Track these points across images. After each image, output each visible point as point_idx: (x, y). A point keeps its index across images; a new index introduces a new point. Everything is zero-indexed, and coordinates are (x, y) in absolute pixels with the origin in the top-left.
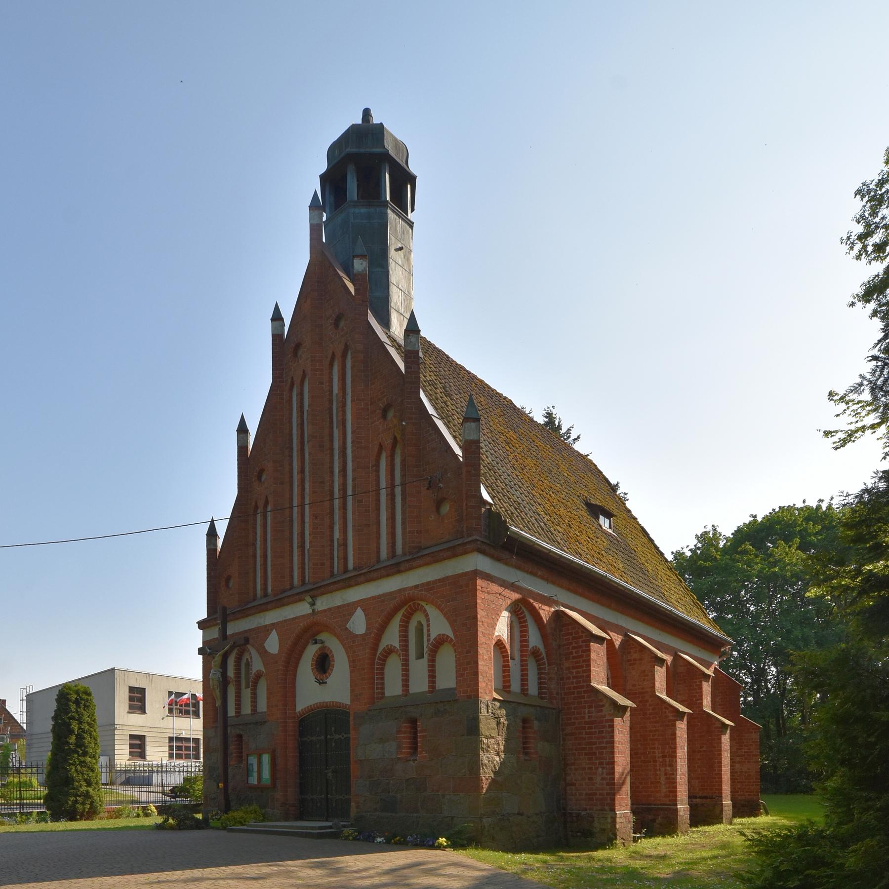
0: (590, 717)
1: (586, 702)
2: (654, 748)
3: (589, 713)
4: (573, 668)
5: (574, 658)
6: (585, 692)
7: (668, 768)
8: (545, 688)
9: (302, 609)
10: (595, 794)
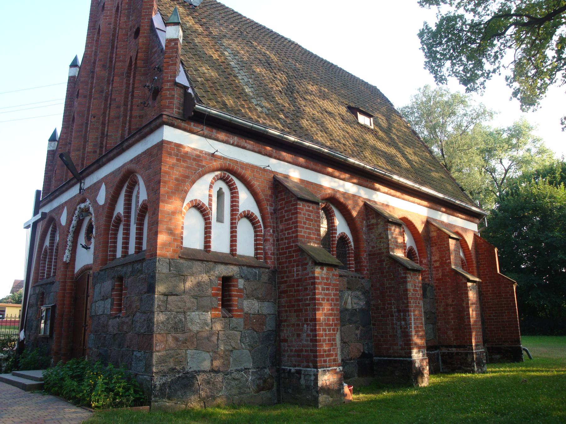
0: (298, 275)
1: (295, 261)
2: (391, 304)
3: (297, 271)
4: (286, 230)
5: (286, 220)
6: (294, 251)
7: (403, 323)
8: (261, 249)
9: (74, 191)
10: (302, 351)
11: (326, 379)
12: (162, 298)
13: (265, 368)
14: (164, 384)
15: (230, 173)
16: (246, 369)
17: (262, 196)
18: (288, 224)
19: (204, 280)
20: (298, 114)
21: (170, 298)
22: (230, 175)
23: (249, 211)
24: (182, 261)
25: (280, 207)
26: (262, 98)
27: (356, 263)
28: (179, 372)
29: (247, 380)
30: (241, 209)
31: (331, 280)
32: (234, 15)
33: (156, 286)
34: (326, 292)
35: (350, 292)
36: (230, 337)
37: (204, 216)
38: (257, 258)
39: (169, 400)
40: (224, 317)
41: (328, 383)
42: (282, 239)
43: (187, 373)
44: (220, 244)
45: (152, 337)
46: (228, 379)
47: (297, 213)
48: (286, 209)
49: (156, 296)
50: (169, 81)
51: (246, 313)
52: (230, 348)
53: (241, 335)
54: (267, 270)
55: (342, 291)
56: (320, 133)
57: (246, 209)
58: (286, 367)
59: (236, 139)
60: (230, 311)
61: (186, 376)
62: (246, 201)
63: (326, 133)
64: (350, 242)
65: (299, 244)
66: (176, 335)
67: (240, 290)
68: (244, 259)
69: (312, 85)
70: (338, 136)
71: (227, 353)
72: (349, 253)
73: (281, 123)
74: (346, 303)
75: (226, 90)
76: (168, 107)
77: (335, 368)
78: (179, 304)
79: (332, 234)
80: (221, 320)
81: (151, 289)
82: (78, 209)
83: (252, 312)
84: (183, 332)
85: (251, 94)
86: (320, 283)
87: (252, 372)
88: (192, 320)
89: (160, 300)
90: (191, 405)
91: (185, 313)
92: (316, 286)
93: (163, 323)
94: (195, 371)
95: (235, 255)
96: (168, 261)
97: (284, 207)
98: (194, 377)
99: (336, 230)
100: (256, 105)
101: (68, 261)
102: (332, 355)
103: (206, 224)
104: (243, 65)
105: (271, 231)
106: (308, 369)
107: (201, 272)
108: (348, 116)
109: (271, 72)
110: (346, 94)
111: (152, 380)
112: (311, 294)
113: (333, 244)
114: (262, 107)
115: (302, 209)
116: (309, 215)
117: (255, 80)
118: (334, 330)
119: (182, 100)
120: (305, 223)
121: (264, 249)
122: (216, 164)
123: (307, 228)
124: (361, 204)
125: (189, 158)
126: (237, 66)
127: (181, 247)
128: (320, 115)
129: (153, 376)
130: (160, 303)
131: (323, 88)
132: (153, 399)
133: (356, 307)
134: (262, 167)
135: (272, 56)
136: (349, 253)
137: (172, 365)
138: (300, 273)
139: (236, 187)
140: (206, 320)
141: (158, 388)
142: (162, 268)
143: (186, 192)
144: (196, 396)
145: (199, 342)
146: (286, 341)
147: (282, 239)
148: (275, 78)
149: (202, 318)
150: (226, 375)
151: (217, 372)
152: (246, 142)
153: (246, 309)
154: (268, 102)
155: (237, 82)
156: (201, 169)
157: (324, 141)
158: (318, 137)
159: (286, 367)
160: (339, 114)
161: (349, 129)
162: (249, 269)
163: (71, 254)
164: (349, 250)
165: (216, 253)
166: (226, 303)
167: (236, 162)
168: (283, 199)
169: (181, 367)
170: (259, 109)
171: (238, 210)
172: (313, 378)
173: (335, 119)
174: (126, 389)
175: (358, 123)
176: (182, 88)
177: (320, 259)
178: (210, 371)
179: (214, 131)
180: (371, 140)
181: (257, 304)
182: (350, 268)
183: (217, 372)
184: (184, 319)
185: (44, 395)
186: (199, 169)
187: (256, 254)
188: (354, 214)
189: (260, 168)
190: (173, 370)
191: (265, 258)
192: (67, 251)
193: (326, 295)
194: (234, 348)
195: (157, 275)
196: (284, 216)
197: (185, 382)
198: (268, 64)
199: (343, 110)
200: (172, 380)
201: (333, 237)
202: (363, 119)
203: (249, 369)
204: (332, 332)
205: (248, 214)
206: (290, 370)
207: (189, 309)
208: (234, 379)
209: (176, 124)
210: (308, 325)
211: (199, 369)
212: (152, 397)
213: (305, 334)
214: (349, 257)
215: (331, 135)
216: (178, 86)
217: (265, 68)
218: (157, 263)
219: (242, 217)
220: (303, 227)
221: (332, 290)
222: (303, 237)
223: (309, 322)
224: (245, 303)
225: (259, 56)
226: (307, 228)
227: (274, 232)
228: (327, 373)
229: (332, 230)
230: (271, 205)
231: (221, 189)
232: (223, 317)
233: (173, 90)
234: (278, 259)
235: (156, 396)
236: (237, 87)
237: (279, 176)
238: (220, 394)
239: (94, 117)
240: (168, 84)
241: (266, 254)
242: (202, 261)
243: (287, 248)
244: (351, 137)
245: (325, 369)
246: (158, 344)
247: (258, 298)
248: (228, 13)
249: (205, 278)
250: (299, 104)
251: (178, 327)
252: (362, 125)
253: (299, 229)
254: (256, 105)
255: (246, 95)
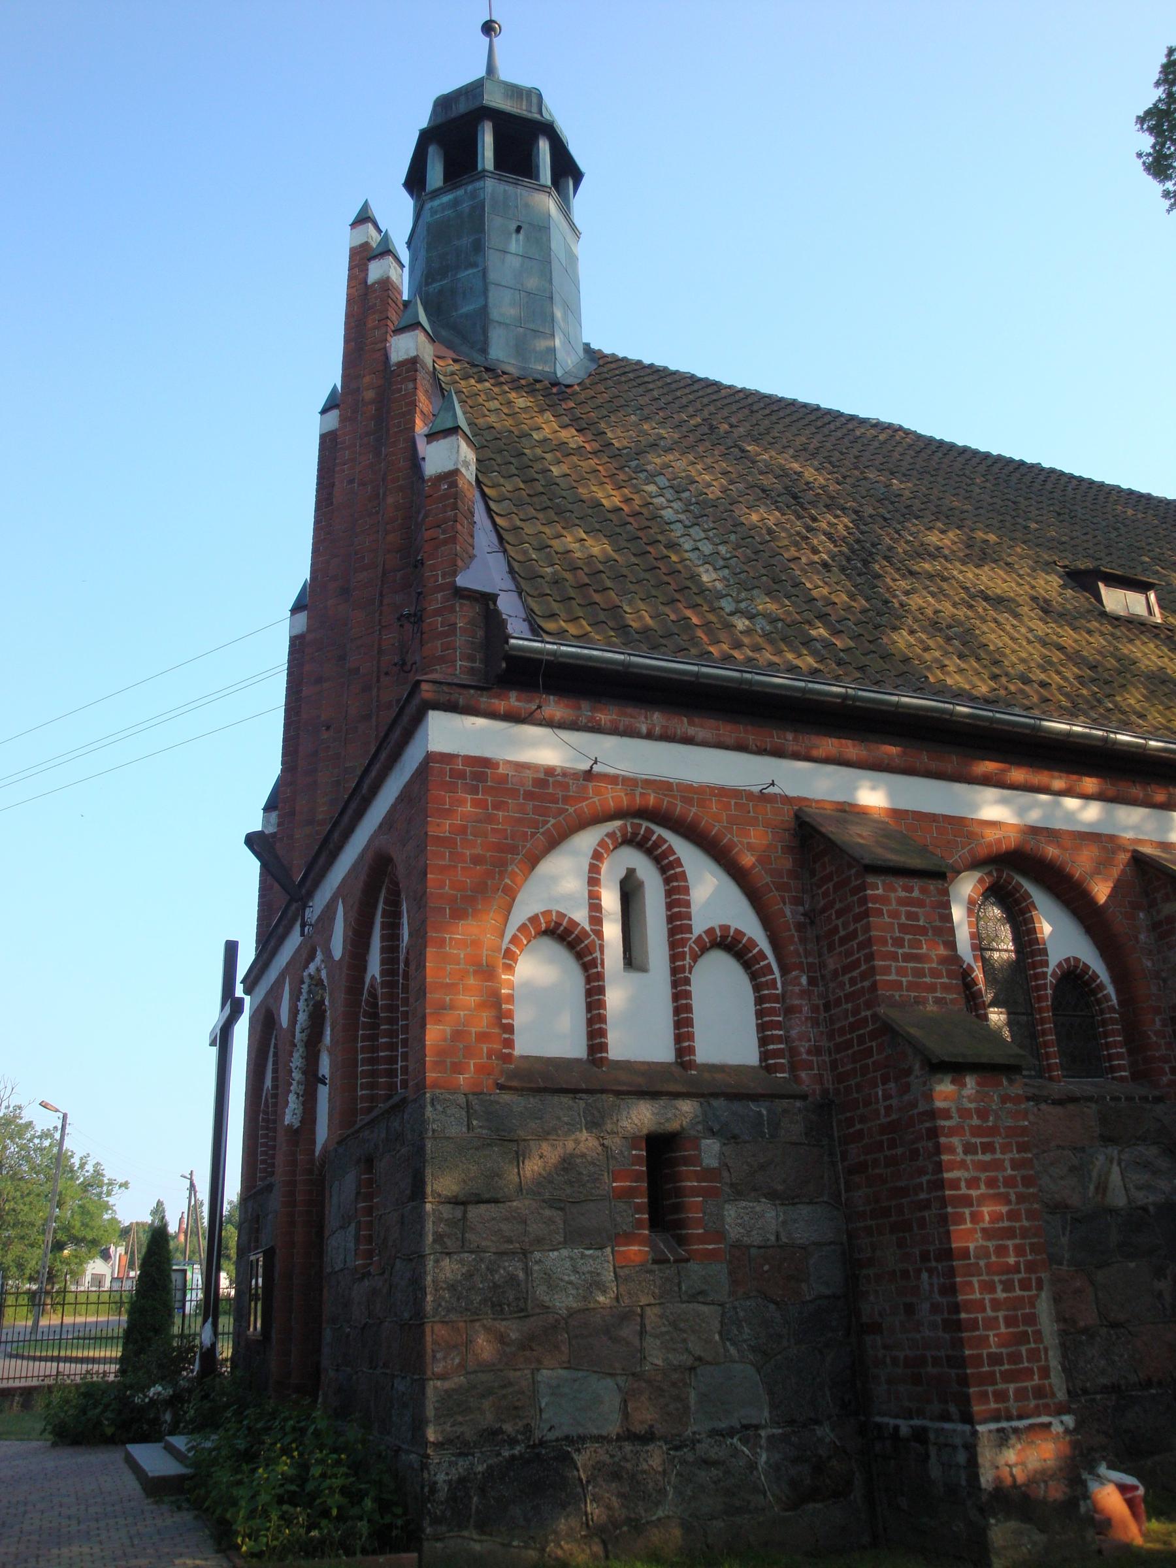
0: (889, 1109)
11: (1022, 1457)
12: (446, 1211)
13: (817, 1422)
14: (462, 1480)
15: (651, 821)
16: (746, 1427)
17: (764, 879)
18: (849, 953)
19: (582, 1148)
20: (883, 620)
21: (474, 1212)
22: (653, 827)
23: (725, 928)
24: (506, 1097)
25: (822, 903)
26: (755, 592)
27: (1131, 1052)
28: (513, 1442)
29: (752, 1466)
30: (699, 926)
31: (997, 1117)
32: (696, 387)
33: (429, 1179)
34: (980, 1157)
35: (1113, 1151)
36: (682, 1325)
37: (579, 956)
38: (769, 1069)
39: (483, 1532)
40: (660, 1261)
41: (1021, 1477)
42: (838, 1002)
43: (542, 1443)
44: (638, 1031)
45: (423, 1334)
46: (683, 1462)
47: (866, 914)
48: (838, 906)
49: (428, 1207)
50: (440, 588)
51: (737, 1246)
52: (685, 1359)
53: (723, 1315)
54: (798, 1104)
55: (1083, 1149)
56: (953, 663)
57: (715, 923)
58: (886, 1420)
59: (657, 719)
60: (681, 1241)
61: (538, 1455)
62: (713, 897)
63: (978, 659)
64: (1101, 987)
65: (881, 1010)
66: (497, 1324)
67: (709, 1174)
68: (718, 1076)
69: (943, 532)
70: (1023, 661)
71: (675, 1376)
72: (1104, 1023)
73: (814, 653)
74: (1102, 1188)
75: (632, 587)
76: (442, 660)
77: (1045, 1419)
78: (504, 1226)
79: (1034, 966)
80: (650, 1272)
81: (418, 1192)
82: (307, 980)
83: (756, 1239)
84: (522, 1313)
85: (719, 585)
86: (952, 1132)
87: (771, 1438)
88: (548, 1276)
89: (441, 1220)
90: (559, 1552)
91: (525, 1253)
92: (943, 1140)
93: (452, 1287)
94: (567, 1438)
95: (603, 1060)
96: (462, 1100)
97: (833, 902)
98: (566, 1459)
99: (1044, 952)
100: (732, 614)
101: (297, 1124)
102: (1029, 1373)
103: (588, 980)
104: (702, 510)
105: (804, 980)
106: (948, 1426)
107: (572, 1127)
108: (1073, 599)
109: (799, 517)
110: (1064, 539)
111: (424, 1466)
112: (930, 1168)
113: (1039, 999)
114: (751, 617)
115: (884, 900)
116: (909, 916)
117: (738, 547)
118: (1025, 1285)
119: (480, 633)
120: (899, 943)
121: (787, 1039)
122: (613, 797)
123: (908, 958)
124: (1123, 857)
125: (513, 793)
126: (682, 517)
127: (508, 1058)
128: (962, 613)
129: (428, 1457)
130: (442, 1228)
131: (980, 535)
132: (428, 1530)
133: (1141, 1198)
134: (756, 789)
135: (810, 474)
136: (1104, 1023)
137: (488, 1419)
138: (894, 1102)
139: (678, 860)
140: (592, 1275)
141: (442, 1495)
142: (444, 1122)
143: (511, 895)
144: (574, 1522)
145: (584, 1340)
146: (875, 1328)
147: (838, 1002)
148: (809, 529)
149: (585, 1269)
150: (677, 1448)
151: (647, 1438)
152: (691, 723)
153: (734, 1232)
154: (775, 599)
155: (674, 558)
156: (552, 821)
157: (970, 682)
158: (948, 673)
159: (886, 1420)
160: (1034, 599)
161: (1068, 637)
162: (736, 1106)
163: (304, 1104)
164: (1102, 1012)
165: (626, 1066)
166: (664, 1213)
167: (664, 786)
168: (828, 878)
169: (520, 1424)
170: (741, 624)
171: (689, 929)
172: (962, 1457)
173: (1016, 616)
174: (353, 1496)
175: (1104, 614)
176: (476, 600)
177: (940, 1050)
178: (619, 1438)
179: (585, 705)
180: (1148, 655)
181: (770, 1214)
182: (1113, 1069)
183: (647, 1438)
184: (521, 1275)
185: (179, 1508)
186: (547, 822)
187: (765, 1056)
188: (1101, 891)
189: (750, 795)
190: (492, 1435)
191: (793, 1068)
192: (292, 1098)
193: (984, 1166)
194: (700, 1359)
195: (429, 1145)
196: (835, 930)
197: (535, 1475)
198: (794, 497)
199: (1050, 585)
200: (490, 1467)
201: (1037, 977)
202: (1115, 600)
203: (757, 1427)
204: (1019, 1293)
205: (724, 937)
206: (896, 1428)
207: (539, 1241)
208: (707, 1463)
209: (461, 702)
210: (931, 1271)
211: (581, 1431)
212: (426, 1523)
213: (926, 1306)
214: (1106, 1034)
215: (996, 663)
216: (462, 597)
217: (777, 508)
218: (429, 1108)
219: (704, 950)
220: (894, 957)
221: (1005, 1148)
222: (898, 985)
223: (934, 1264)
224: (731, 1213)
225: (767, 481)
226: (908, 958)
227: (812, 981)
228: (1013, 1440)
229: (1033, 954)
230: (797, 901)
231: (631, 872)
232: (655, 1262)
233: (452, 609)
234: (834, 1065)
235: (436, 1521)
236: (673, 572)
237: (1147, 850)
238: (660, 1513)
239: (328, 728)
240: (439, 596)
241: (793, 1052)
242: (574, 1092)
243: (853, 1027)
244: (1075, 658)
245: (1004, 1424)
246: (439, 1355)
247: (773, 1196)
248: (674, 386)
249: (586, 1142)
250: (888, 589)
251: (505, 1299)
252: (1117, 618)
253: (879, 963)
254: (732, 614)
255: (702, 590)
